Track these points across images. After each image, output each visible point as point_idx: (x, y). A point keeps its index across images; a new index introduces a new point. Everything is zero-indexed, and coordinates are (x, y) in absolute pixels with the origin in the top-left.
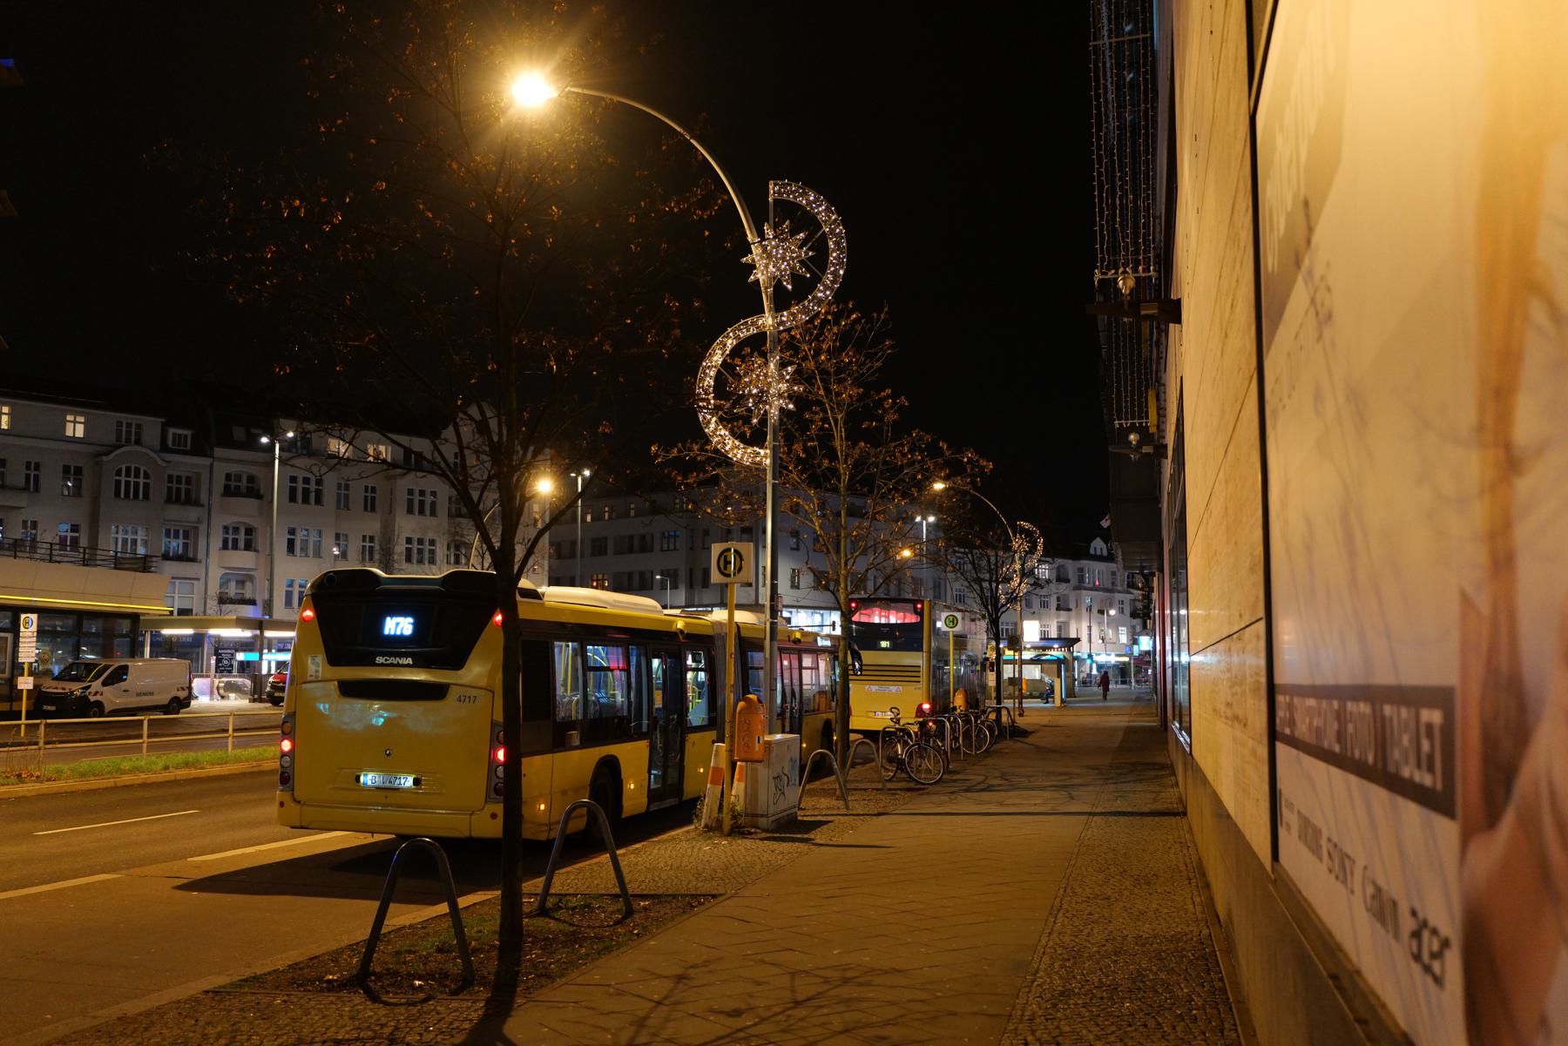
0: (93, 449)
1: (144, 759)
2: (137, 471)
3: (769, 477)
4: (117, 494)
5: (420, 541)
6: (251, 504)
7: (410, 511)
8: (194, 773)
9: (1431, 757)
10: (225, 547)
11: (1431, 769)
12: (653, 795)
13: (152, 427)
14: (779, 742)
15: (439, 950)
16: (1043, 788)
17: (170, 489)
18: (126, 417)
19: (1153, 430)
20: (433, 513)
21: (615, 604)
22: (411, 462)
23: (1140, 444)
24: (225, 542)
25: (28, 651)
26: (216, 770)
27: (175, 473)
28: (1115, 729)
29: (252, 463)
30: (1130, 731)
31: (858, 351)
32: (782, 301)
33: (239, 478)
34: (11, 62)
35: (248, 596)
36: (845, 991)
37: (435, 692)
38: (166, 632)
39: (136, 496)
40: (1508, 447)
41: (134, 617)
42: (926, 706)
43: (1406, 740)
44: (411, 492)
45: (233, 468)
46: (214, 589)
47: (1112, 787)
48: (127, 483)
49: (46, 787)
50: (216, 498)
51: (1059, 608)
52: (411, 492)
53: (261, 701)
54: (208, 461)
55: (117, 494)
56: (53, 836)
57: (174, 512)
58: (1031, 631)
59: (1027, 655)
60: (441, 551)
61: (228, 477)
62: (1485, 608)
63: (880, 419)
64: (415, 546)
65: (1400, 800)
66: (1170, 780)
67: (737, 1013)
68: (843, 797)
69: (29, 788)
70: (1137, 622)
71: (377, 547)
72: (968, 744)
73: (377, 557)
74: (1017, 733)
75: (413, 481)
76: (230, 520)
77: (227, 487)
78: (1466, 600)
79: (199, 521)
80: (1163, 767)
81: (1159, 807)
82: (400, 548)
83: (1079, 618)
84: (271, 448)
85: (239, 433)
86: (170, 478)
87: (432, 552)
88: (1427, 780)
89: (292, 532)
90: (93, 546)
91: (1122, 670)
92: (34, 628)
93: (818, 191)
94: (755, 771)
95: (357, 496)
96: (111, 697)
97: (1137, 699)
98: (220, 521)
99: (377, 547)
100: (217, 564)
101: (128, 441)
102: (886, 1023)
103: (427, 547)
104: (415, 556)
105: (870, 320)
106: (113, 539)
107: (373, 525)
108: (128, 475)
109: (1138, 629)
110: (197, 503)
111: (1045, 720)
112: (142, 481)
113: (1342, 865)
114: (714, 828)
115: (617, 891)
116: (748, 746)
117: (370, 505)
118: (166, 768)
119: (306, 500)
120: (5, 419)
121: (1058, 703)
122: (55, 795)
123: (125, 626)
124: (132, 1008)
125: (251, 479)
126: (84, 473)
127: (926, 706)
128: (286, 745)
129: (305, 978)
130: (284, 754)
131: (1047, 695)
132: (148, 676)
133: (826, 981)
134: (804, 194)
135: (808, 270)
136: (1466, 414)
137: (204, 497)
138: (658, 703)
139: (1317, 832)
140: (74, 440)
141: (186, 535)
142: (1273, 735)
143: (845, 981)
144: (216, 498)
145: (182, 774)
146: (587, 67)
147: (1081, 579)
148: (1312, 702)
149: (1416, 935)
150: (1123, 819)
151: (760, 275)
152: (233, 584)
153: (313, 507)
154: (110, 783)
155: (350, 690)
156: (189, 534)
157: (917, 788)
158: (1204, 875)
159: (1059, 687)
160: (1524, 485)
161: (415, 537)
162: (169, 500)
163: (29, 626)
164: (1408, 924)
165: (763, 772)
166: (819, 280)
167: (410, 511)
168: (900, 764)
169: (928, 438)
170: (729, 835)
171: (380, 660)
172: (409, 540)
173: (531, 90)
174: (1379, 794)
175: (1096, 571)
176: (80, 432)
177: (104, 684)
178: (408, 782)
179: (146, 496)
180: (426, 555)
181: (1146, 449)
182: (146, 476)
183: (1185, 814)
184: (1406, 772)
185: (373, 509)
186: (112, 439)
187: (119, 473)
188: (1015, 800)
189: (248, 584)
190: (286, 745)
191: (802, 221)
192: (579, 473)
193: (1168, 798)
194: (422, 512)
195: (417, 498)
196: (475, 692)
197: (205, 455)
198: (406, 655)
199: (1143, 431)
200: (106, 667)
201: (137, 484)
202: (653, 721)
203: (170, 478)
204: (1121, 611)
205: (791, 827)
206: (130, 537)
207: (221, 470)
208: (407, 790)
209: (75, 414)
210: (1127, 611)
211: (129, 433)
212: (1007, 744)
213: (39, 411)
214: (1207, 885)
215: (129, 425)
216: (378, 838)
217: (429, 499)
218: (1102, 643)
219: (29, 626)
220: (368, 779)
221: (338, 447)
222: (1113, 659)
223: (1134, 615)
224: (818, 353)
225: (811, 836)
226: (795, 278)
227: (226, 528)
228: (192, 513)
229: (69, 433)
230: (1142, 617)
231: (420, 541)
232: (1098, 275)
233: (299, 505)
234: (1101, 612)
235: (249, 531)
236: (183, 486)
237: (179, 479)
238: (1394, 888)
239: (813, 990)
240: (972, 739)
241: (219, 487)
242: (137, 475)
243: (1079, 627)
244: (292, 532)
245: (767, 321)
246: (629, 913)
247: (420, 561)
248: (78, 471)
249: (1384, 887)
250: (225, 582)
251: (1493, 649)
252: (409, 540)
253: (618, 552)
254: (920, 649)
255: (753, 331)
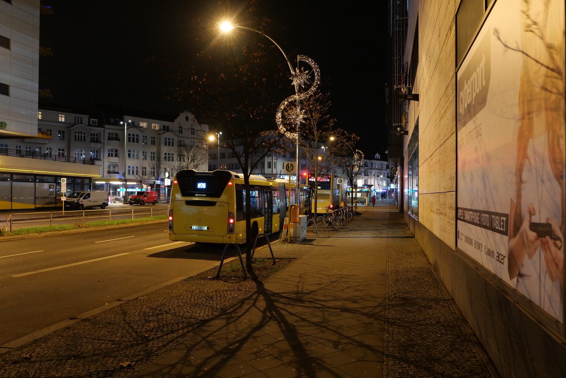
1: (111, 221)
2: (81, 132)
3: (297, 142)
4: (76, 139)
6: (117, 142)
7: (166, 145)
8: (126, 225)
9: (503, 226)
11: (503, 227)
12: (265, 232)
13: (85, 118)
15: (232, 271)
17: (91, 138)
18: (77, 115)
19: (404, 126)
20: (173, 145)
22: (165, 129)
23: (401, 131)
24: (109, 154)
25: (64, 189)
26: (131, 225)
28: (386, 213)
30: (390, 213)
32: (301, 90)
35: (116, 171)
36: (343, 279)
37: (213, 204)
38: (97, 182)
40: (521, 179)
41: (90, 179)
42: (331, 206)
43: (497, 222)
44: (166, 139)
45: (111, 131)
46: (106, 169)
48: (79, 136)
49: (88, 229)
52: (166, 139)
53: (127, 203)
54: (103, 129)
55: (76, 139)
56: (101, 243)
57: (93, 145)
58: (360, 183)
59: (358, 190)
60: (175, 157)
61: (109, 134)
62: (515, 202)
63: (328, 125)
64: (167, 156)
65: (496, 233)
70: (389, 179)
71: (156, 156)
73: (156, 159)
74: (358, 214)
75: (168, 135)
77: (109, 137)
78: (511, 200)
79: (101, 148)
80: (404, 224)
81: (406, 235)
82: (163, 156)
83: (371, 178)
84: (124, 125)
85: (112, 120)
87: (173, 157)
88: (502, 229)
89: (129, 151)
90: (69, 156)
92: (66, 182)
94: (296, 225)
95: (149, 140)
96: (86, 203)
97: (390, 203)
98: (107, 148)
99: (156, 156)
100: (107, 161)
101: (78, 123)
102: (357, 286)
104: (167, 159)
105: (325, 95)
106: (74, 153)
107: (154, 149)
108: (79, 133)
109: (389, 182)
110: (100, 142)
111: (364, 210)
112: (83, 135)
113: (478, 246)
114: (285, 241)
115: (271, 257)
117: (153, 143)
118: (118, 224)
119: (133, 141)
120: (40, 116)
121: (367, 204)
122: (91, 232)
123: (87, 181)
125: (116, 135)
126: (65, 132)
128: (171, 218)
129: (202, 277)
130: (170, 221)
131: (363, 202)
132: (96, 197)
133: (337, 277)
134: (308, 59)
135: (309, 82)
136: (514, 170)
137: (102, 141)
139: (471, 240)
140: (61, 122)
141: (97, 152)
142: (457, 219)
143: (342, 278)
145: (123, 226)
146: (241, 19)
147: (372, 166)
148: (471, 213)
149: (498, 256)
151: (295, 83)
152: (112, 167)
153: (135, 143)
154: (105, 228)
155: (189, 203)
156: (98, 152)
157: (335, 230)
158: (424, 253)
159: (367, 200)
160: (523, 186)
162: (91, 141)
163: (64, 182)
164: (496, 255)
166: (312, 85)
167: (166, 145)
168: (330, 223)
169: (342, 130)
171: (196, 195)
172: (165, 154)
173: (226, 27)
174: (489, 232)
175: (377, 164)
176: (63, 120)
177: (84, 199)
178: (206, 228)
179: (84, 140)
180: (171, 159)
181: (402, 132)
182: (84, 134)
183: (414, 237)
184: (497, 228)
185: (154, 144)
186: (73, 122)
187: (76, 133)
189: (116, 168)
191: (308, 67)
193: (408, 233)
194: (169, 145)
195: (168, 141)
196: (223, 204)
197: (102, 127)
198: (204, 194)
199: (401, 127)
200: (83, 194)
201: (81, 136)
202: (265, 212)
203: (91, 134)
204: (384, 176)
205: (306, 241)
207: (107, 132)
208: (205, 230)
209: (62, 114)
210: (386, 176)
211: (78, 120)
212: (355, 217)
213: (51, 113)
214: (426, 256)
215: (78, 118)
216: (189, 243)
218: (378, 185)
219: (64, 182)
220: (194, 227)
221: (144, 125)
223: (388, 177)
224: (309, 105)
227: (109, 151)
228: (98, 146)
229: (60, 120)
230: (391, 178)
231: (169, 154)
233: (132, 143)
234: (378, 176)
236: (95, 137)
237: (94, 134)
238: (492, 248)
239: (335, 280)
242: (81, 134)
243: (371, 181)
245: (296, 97)
246: (275, 262)
247: (169, 160)
248: (63, 132)
249: (490, 249)
250: (109, 167)
251: (516, 209)
252: (165, 154)
253: (229, 157)
254: (329, 189)
255: (293, 99)
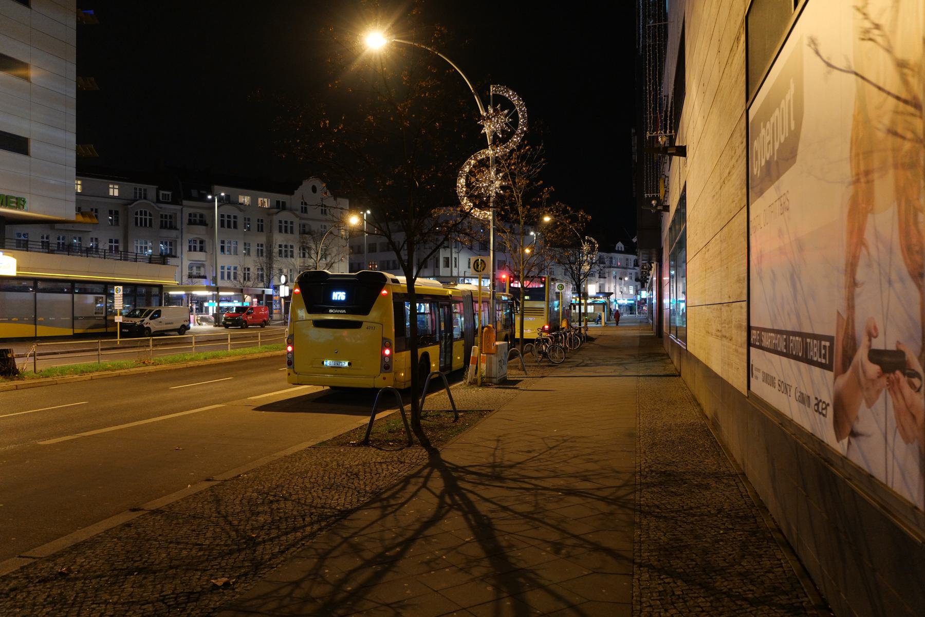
0: (126, 202)
2: (146, 212)
3: (491, 224)
4: (136, 224)
5: (286, 246)
6: (202, 228)
7: (280, 231)
9: (825, 355)
10: (190, 250)
11: (825, 358)
12: (441, 369)
13: (151, 190)
14: (500, 345)
16: (611, 365)
18: (139, 186)
19: (662, 198)
21: (425, 284)
24: (190, 247)
26: (228, 359)
27: (164, 214)
29: (199, 208)
30: (641, 337)
31: (528, 164)
32: (496, 141)
33: (195, 216)
34: (92, 12)
35: (202, 274)
37: (357, 325)
39: (146, 225)
40: (854, 279)
41: (160, 287)
42: (547, 327)
43: (815, 350)
44: (280, 222)
45: (192, 211)
46: (186, 272)
47: (643, 364)
48: (141, 219)
50: (185, 226)
51: (600, 277)
55: (136, 224)
56: (180, 389)
57: (166, 233)
58: (592, 289)
59: (589, 301)
60: (296, 251)
61: (190, 215)
62: (845, 317)
63: (541, 197)
66: (669, 361)
67: (529, 452)
68: (524, 370)
69: (151, 368)
71: (265, 250)
72: (570, 346)
73: (264, 254)
74: (589, 339)
76: (192, 237)
77: (190, 220)
79: (177, 238)
80: (663, 355)
82: (276, 250)
83: (610, 282)
85: (194, 193)
86: (162, 216)
87: (292, 252)
88: (823, 361)
89: (223, 242)
90: (126, 250)
91: (631, 308)
92: (121, 293)
93: (514, 90)
95: (254, 224)
96: (154, 325)
98: (188, 237)
99: (265, 250)
100: (187, 258)
101: (140, 198)
103: (289, 249)
105: (535, 150)
107: (262, 239)
108: (141, 214)
109: (639, 287)
110: (176, 228)
111: (600, 333)
112: (148, 217)
113: (785, 388)
114: (474, 383)
115: (451, 408)
116: (489, 347)
117: (260, 229)
119: (229, 226)
121: (603, 324)
124: (289, 452)
125: (201, 216)
126: (120, 214)
127: (547, 327)
129: (341, 441)
130: (289, 353)
132: (170, 315)
133: (557, 441)
134: (507, 92)
135: (509, 127)
137: (179, 226)
138: (443, 329)
140: (113, 197)
141: (171, 244)
142: (749, 344)
143: (565, 441)
144: (185, 226)
146: (400, 28)
147: (611, 262)
148: (772, 335)
149: (817, 405)
150: (653, 378)
152: (195, 268)
154: (184, 365)
155: (318, 324)
156: (172, 243)
157: (553, 365)
158: (696, 400)
160: (858, 290)
161: (283, 244)
162: (161, 227)
163: (118, 292)
164: (813, 402)
165: (494, 359)
168: (545, 355)
169: (563, 206)
170: (481, 386)
171: (331, 311)
172: (280, 246)
173: (375, 41)
174: (803, 365)
175: (619, 258)
176: (116, 194)
177: (151, 319)
178: (346, 364)
179: (151, 225)
180: (289, 254)
181: (659, 208)
182: (150, 215)
184: (815, 359)
185: (262, 231)
186: (132, 196)
187: (137, 214)
188: (600, 370)
189: (202, 269)
190: (290, 349)
191: (507, 104)
192: (365, 211)
193: (671, 369)
194: (286, 232)
195: (283, 225)
199: (657, 199)
201: (146, 219)
202: (441, 338)
203: (162, 216)
204: (631, 278)
205: (505, 383)
206: (143, 245)
207: (187, 211)
208: (345, 368)
209: (114, 184)
210: (634, 278)
211: (140, 194)
212: (586, 344)
213: (96, 182)
214: (699, 405)
215: (140, 189)
216: (320, 389)
217: (289, 225)
218: (622, 294)
219: (118, 292)
220: (328, 363)
221: (245, 200)
222: (626, 302)
223: (637, 280)
224: (509, 165)
225: (517, 386)
226: (503, 131)
228: (173, 234)
229: (111, 194)
230: (642, 282)
231: (286, 246)
232: (648, 134)
234: (621, 279)
235: (201, 242)
236: (168, 220)
237: (166, 216)
238: (808, 391)
239: (554, 444)
240: (569, 344)
241: (186, 220)
242: (146, 215)
244: (223, 242)
245: (490, 152)
246: (457, 418)
247: (286, 256)
248: (117, 213)
250: (191, 268)
251: (847, 329)
252: (280, 246)
253: (382, 250)
255: (484, 156)
